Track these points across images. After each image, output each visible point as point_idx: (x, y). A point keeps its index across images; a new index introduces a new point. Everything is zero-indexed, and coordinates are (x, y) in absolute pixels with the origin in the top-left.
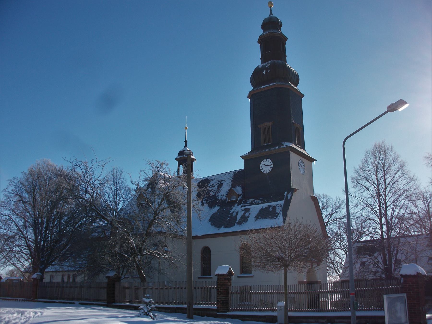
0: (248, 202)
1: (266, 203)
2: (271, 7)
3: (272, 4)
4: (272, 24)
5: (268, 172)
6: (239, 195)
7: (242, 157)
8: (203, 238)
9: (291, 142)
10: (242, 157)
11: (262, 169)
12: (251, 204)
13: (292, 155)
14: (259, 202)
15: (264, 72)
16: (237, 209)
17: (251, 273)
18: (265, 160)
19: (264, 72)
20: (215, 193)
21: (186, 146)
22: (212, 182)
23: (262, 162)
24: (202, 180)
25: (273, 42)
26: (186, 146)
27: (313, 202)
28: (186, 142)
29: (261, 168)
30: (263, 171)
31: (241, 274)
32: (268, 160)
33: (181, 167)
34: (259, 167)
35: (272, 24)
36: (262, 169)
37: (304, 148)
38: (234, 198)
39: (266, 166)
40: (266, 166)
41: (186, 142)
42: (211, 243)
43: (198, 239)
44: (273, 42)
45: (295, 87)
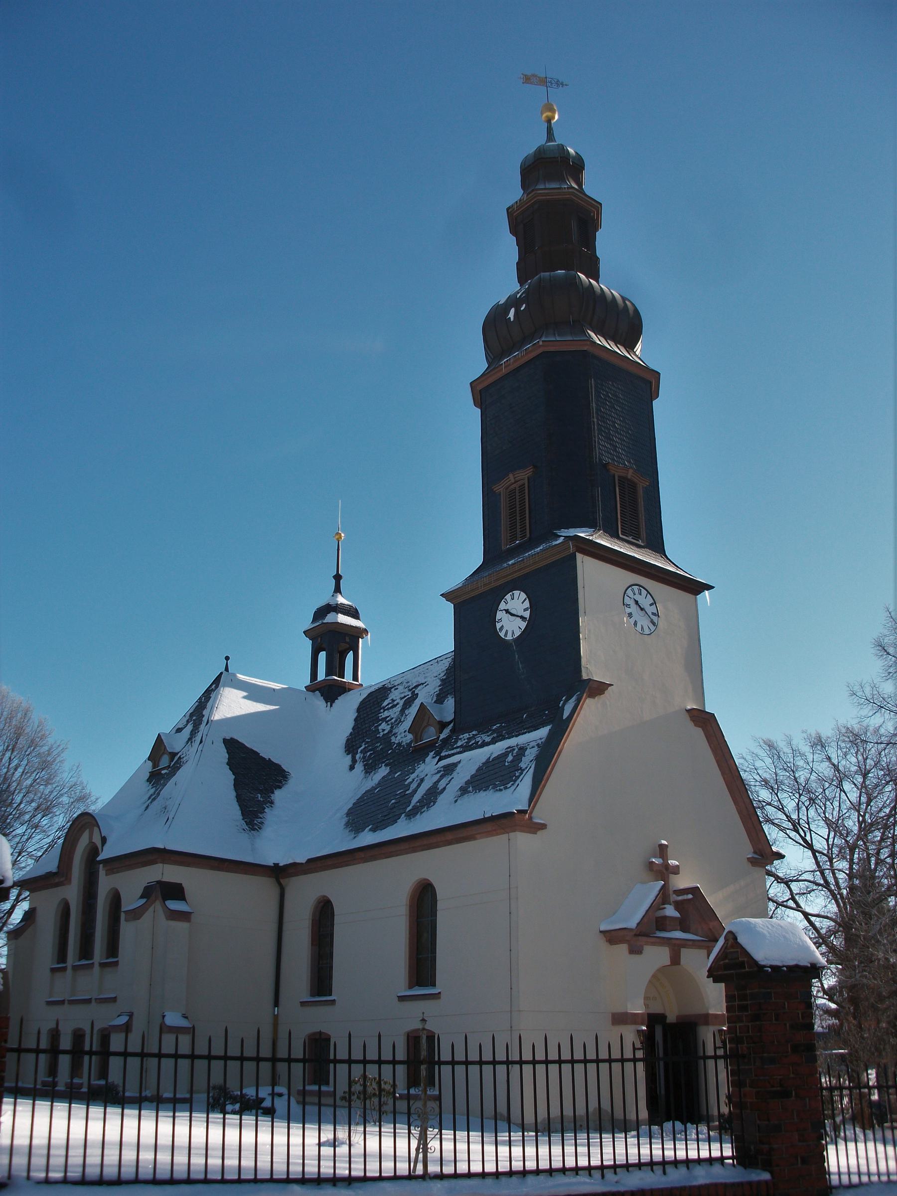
0: (459, 744)
1: (504, 739)
2: (549, 121)
3: (554, 112)
4: (551, 167)
5: (518, 633)
6: (442, 725)
7: (447, 596)
8: (316, 870)
9: (592, 524)
10: (447, 596)
11: (502, 628)
12: (467, 748)
13: (586, 566)
14: (488, 739)
15: (511, 314)
16: (429, 767)
17: (434, 985)
18: (508, 597)
19: (511, 314)
20: (392, 727)
21: (338, 590)
22: (395, 695)
23: (502, 606)
24: (372, 689)
25: (555, 220)
26: (338, 590)
27: (698, 733)
28: (338, 578)
29: (498, 626)
30: (502, 634)
31: (411, 987)
32: (516, 593)
33: (322, 656)
34: (494, 622)
35: (551, 167)
36: (502, 628)
37: (657, 545)
38: (430, 734)
39: (513, 616)
40: (513, 616)
41: (338, 578)
42: (332, 884)
43: (296, 874)
44: (555, 220)
45: (621, 351)
